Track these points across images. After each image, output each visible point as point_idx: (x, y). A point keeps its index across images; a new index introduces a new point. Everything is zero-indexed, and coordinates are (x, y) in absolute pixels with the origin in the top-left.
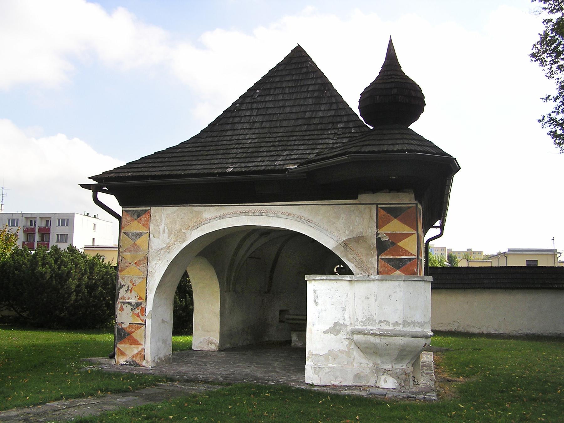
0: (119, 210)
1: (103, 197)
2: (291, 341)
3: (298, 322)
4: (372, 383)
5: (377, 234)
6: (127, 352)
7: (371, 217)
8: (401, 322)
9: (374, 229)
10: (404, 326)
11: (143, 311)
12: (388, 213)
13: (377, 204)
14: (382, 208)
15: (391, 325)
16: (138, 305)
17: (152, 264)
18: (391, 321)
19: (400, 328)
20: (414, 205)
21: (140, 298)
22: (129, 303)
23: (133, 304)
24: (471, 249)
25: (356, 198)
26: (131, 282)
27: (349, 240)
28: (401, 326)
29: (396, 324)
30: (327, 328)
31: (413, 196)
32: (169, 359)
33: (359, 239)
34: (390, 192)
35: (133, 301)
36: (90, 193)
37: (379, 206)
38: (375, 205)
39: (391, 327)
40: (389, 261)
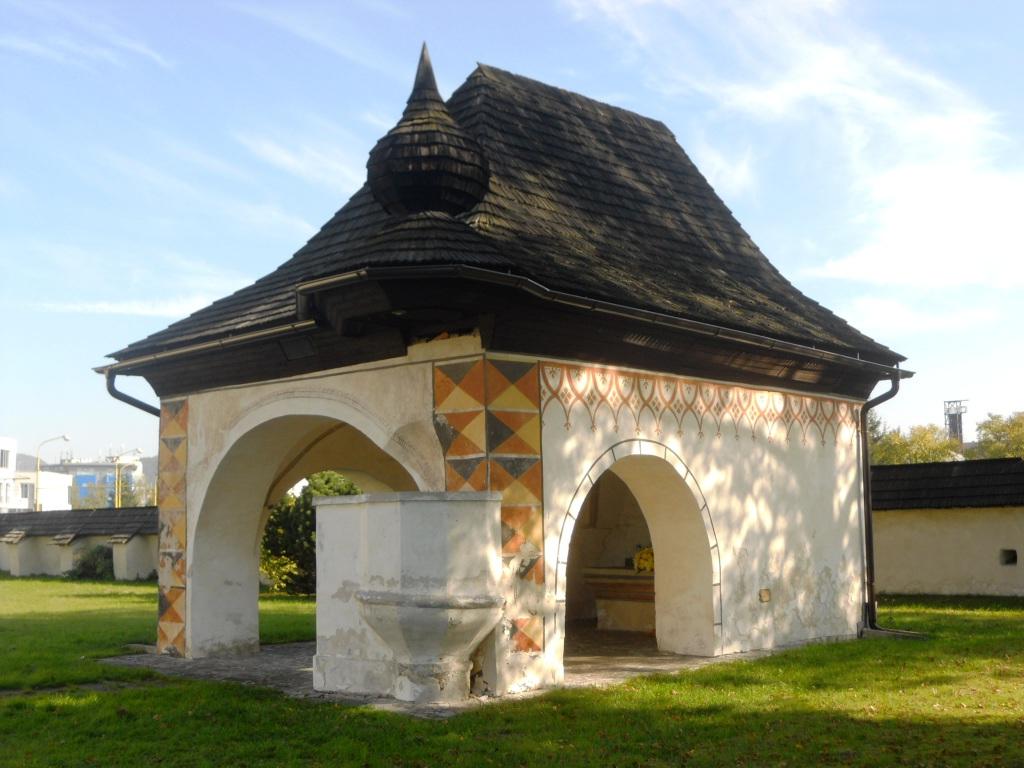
0: (154, 401)
1: (123, 383)
2: (596, 619)
3: (621, 581)
4: (405, 692)
5: (435, 416)
6: (168, 634)
7: (425, 386)
8: (398, 578)
9: (430, 408)
10: (403, 586)
11: (184, 565)
12: (448, 376)
13: (434, 361)
14: (440, 368)
15: (386, 584)
16: (179, 555)
17: (190, 489)
18: (387, 577)
19: (397, 589)
20: (481, 358)
21: (181, 546)
22: (170, 554)
23: (174, 555)
24: (999, 417)
25: (404, 353)
26: (171, 520)
27: (402, 429)
28: (399, 586)
29: (392, 582)
30: (335, 591)
31: (478, 339)
32: (250, 647)
33: (414, 427)
34: (449, 337)
35: (173, 550)
36: (103, 379)
37: (437, 364)
38: (430, 364)
39: (384, 589)
40: (504, 462)
